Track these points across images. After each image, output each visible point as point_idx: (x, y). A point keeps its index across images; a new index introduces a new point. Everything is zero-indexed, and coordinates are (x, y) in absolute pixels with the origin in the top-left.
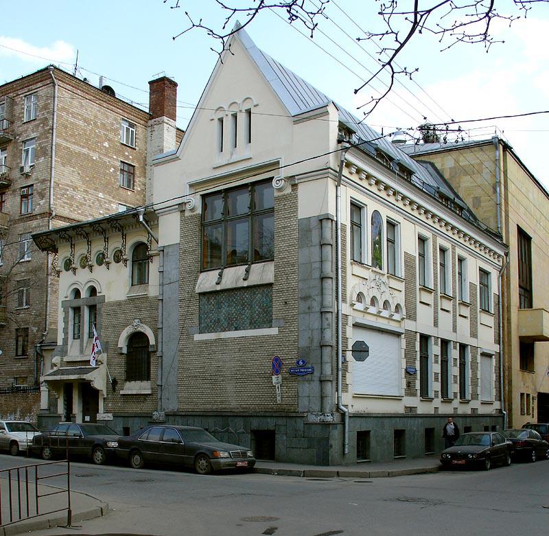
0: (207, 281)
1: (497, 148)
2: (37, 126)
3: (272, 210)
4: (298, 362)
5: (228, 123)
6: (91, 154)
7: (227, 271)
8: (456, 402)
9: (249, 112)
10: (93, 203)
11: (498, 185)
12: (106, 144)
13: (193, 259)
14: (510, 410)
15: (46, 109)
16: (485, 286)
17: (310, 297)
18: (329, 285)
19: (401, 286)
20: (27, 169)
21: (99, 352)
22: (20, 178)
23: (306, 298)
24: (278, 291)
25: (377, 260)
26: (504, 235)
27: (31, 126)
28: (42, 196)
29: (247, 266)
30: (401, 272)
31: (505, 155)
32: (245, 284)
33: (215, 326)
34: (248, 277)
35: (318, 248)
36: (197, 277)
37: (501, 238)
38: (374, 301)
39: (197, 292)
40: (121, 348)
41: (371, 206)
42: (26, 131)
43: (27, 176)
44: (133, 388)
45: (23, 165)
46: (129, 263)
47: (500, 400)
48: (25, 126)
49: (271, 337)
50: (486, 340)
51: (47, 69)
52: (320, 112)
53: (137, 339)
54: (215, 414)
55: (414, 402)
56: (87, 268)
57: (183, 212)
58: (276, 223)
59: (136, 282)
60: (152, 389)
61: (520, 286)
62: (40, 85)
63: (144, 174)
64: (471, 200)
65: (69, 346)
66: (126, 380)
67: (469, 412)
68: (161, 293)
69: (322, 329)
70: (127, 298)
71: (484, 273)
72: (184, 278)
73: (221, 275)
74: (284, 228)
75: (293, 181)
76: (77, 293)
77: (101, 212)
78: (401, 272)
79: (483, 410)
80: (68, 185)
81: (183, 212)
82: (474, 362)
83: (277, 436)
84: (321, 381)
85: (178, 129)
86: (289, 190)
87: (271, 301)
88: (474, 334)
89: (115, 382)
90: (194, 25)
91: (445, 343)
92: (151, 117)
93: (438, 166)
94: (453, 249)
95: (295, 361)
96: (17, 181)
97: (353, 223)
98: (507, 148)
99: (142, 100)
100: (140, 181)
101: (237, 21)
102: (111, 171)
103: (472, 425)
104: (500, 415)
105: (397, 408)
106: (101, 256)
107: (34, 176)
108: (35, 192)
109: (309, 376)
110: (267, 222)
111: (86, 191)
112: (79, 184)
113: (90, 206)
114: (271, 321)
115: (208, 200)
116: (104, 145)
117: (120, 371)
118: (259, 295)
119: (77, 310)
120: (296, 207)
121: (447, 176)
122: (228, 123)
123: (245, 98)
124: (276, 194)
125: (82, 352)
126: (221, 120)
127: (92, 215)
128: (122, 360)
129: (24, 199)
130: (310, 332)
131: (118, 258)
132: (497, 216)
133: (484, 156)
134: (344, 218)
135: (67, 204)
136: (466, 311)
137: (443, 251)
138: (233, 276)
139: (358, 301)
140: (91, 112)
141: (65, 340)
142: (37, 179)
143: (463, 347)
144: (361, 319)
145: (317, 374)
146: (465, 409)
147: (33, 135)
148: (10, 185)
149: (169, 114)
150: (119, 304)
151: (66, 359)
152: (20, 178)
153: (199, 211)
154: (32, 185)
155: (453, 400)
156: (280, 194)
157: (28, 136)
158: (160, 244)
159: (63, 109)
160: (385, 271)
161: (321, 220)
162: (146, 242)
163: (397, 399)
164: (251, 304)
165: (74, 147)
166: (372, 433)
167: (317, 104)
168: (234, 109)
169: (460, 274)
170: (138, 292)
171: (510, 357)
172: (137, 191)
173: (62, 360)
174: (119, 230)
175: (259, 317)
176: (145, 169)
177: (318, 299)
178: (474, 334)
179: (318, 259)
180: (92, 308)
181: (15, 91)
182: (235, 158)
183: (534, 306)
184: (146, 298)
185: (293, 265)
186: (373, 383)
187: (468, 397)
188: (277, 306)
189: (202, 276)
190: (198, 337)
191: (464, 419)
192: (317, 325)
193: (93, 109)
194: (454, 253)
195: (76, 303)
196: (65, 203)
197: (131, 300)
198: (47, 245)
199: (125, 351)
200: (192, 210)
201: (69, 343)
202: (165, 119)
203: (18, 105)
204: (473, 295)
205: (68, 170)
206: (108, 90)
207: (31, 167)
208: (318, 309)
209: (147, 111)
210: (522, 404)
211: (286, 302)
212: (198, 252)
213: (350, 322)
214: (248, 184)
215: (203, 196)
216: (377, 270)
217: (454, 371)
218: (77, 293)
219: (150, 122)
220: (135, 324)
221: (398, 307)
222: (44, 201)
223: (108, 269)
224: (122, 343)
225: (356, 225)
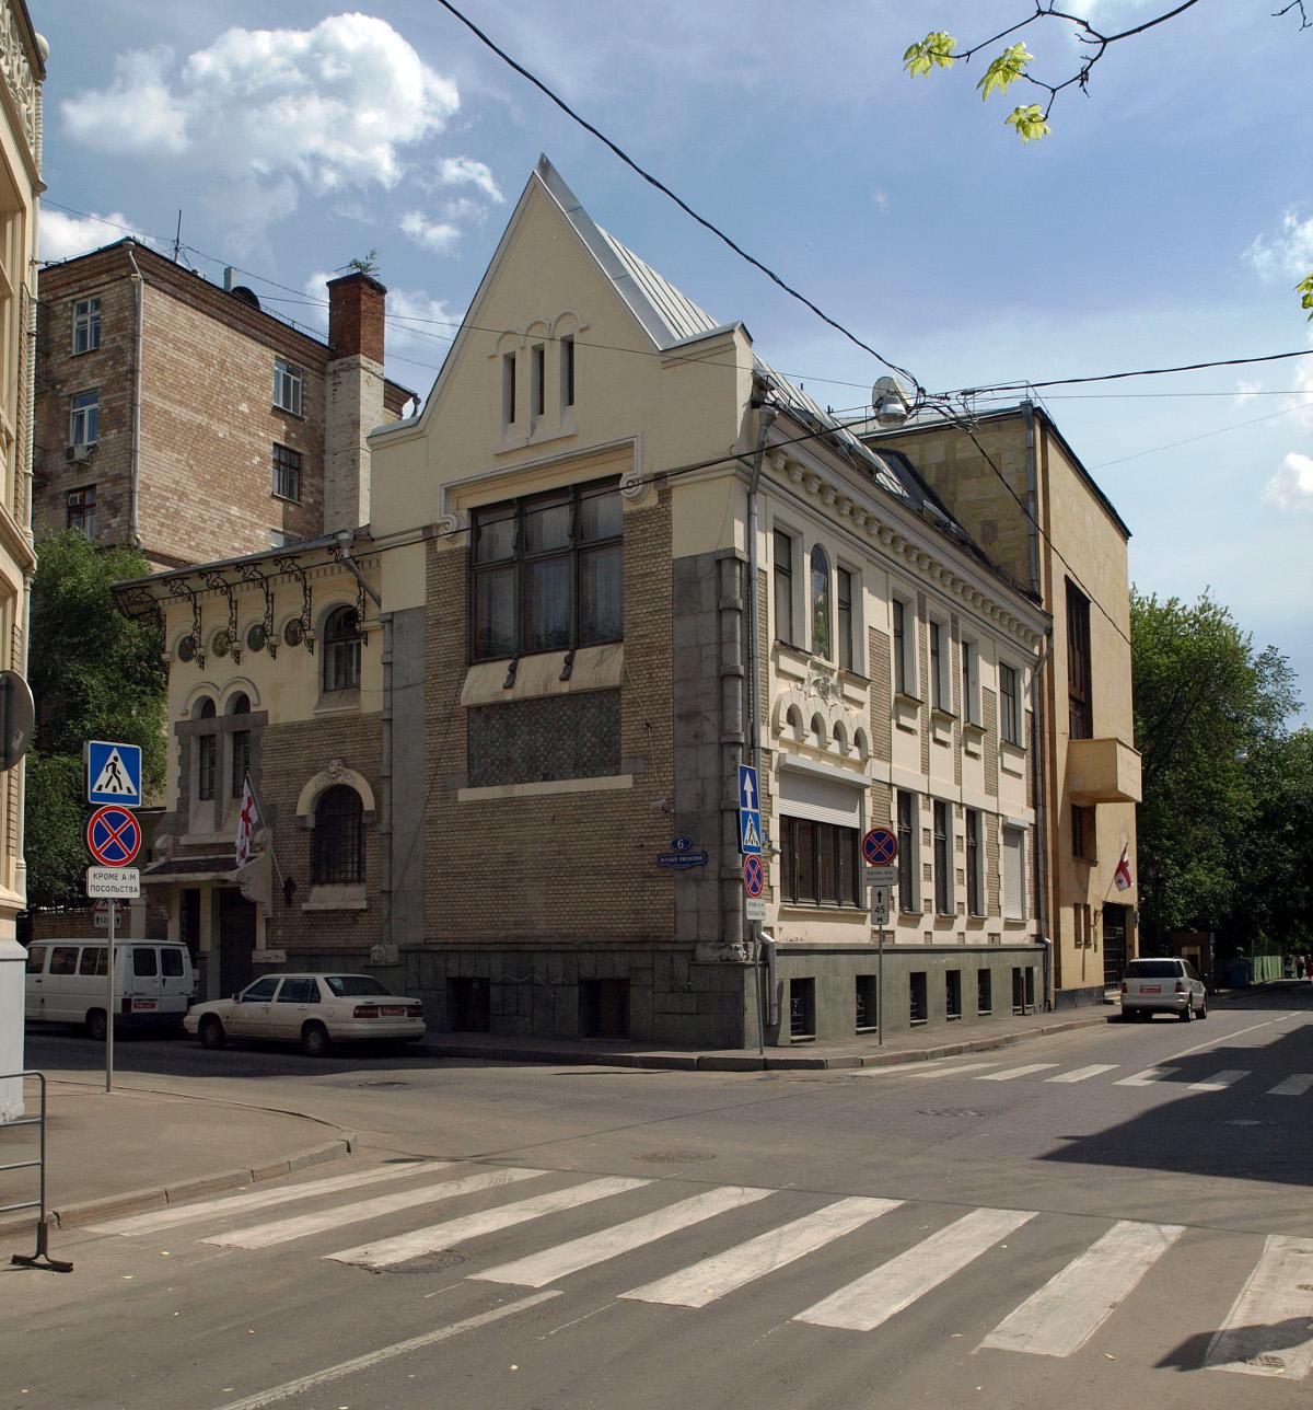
0: (484, 683)
2: (101, 365)
3: (616, 541)
4: (674, 844)
6: (215, 426)
7: (524, 662)
9: (569, 345)
10: (220, 527)
11: (1028, 501)
12: (244, 407)
13: (453, 639)
15: (119, 330)
20: (80, 454)
21: (258, 826)
22: (66, 471)
23: (689, 716)
24: (632, 702)
25: (822, 640)
26: (1043, 596)
27: (87, 364)
28: (114, 508)
29: (567, 653)
32: (565, 688)
33: (504, 771)
34: (513, 682)
35: (714, 615)
36: (463, 675)
37: (1038, 600)
39: (462, 704)
40: (303, 818)
41: (811, 535)
42: (77, 373)
43: (81, 466)
44: (327, 897)
45: (72, 444)
48: (75, 364)
49: (619, 793)
50: (1014, 803)
51: (118, 245)
53: (337, 800)
54: (504, 947)
56: (228, 655)
60: (369, 900)
61: (1071, 697)
62: (105, 278)
63: (320, 470)
64: (978, 527)
65: (191, 813)
68: (388, 705)
69: (722, 777)
70: (313, 717)
72: (435, 676)
73: (513, 670)
76: (207, 707)
77: (236, 545)
80: (167, 489)
84: (721, 881)
85: (387, 381)
86: (651, 500)
87: (618, 722)
89: (290, 886)
90: (1105, 41)
91: (941, 808)
93: (914, 460)
94: (955, 620)
95: (668, 841)
96: (58, 477)
97: (778, 569)
98: (1048, 427)
99: (316, 319)
100: (312, 485)
101: (543, 155)
102: (255, 462)
103: (991, 967)
104: (1039, 945)
106: (258, 631)
107: (96, 468)
108: (99, 501)
109: (696, 871)
111: (203, 502)
112: (191, 486)
113: (213, 533)
114: (618, 762)
115: (482, 520)
116: (240, 408)
117: (299, 861)
118: (593, 710)
119: (207, 741)
120: (669, 534)
121: (930, 480)
123: (563, 311)
125: (218, 825)
126: (511, 361)
127: (217, 551)
128: (305, 840)
129: (75, 515)
130: (700, 783)
131: (294, 635)
132: (1029, 558)
133: (1000, 443)
134: (765, 556)
135: (168, 527)
138: (539, 674)
140: (213, 339)
141: (183, 803)
142: (104, 474)
143: (973, 816)
144: (804, 761)
145: (713, 865)
146: (978, 938)
147: (93, 383)
148: (45, 485)
149: (370, 349)
150: (297, 729)
151: (184, 840)
152: (66, 471)
154: (92, 487)
155: (956, 917)
156: (634, 508)
157: (81, 384)
158: (387, 607)
159: (158, 332)
160: (835, 664)
161: (719, 562)
162: (355, 604)
164: (578, 732)
165: (176, 410)
166: (817, 982)
167: (704, 329)
169: (966, 670)
170: (338, 708)
172: (308, 504)
173: (176, 842)
174: (297, 579)
175: (593, 753)
176: (323, 461)
177: (713, 716)
178: (992, 789)
179: (713, 638)
180: (240, 738)
181: (51, 290)
182: (542, 434)
183: (1095, 734)
184: (355, 719)
185: (663, 651)
188: (629, 733)
189: (475, 673)
190: (466, 795)
191: (977, 955)
192: (711, 769)
193: (214, 335)
195: (206, 727)
196: (162, 525)
197: (321, 724)
198: (141, 608)
199: (311, 823)
201: (192, 807)
202: (363, 360)
203: (57, 318)
205: (167, 457)
206: (246, 297)
207: (89, 448)
208: (714, 738)
209: (326, 342)
210: (1077, 924)
211: (648, 725)
214: (510, 500)
215: (475, 512)
216: (821, 660)
217: (959, 860)
218: (207, 707)
219: (333, 366)
220: (333, 769)
222: (118, 519)
223: (275, 657)
224: (304, 806)
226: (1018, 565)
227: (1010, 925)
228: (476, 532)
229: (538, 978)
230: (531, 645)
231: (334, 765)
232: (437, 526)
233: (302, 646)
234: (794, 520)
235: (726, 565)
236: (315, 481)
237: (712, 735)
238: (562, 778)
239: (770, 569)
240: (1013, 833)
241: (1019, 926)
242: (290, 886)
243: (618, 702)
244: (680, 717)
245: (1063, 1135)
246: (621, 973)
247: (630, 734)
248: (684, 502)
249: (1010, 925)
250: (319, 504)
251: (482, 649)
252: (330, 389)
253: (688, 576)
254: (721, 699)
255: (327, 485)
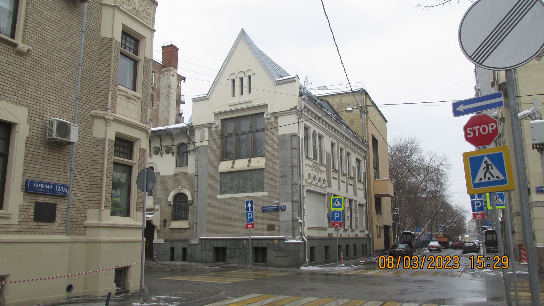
0: (225, 166)
1: (362, 94)
5: (237, 82)
8: (349, 231)
9: (250, 77)
13: (216, 154)
14: (372, 235)
16: (359, 167)
17: (286, 176)
18: (296, 169)
19: (324, 169)
23: (283, 177)
25: (315, 155)
30: (325, 162)
31: (366, 98)
33: (231, 190)
35: (290, 150)
38: (315, 177)
41: (312, 128)
44: (175, 224)
46: (175, 154)
47: (368, 229)
49: (263, 197)
50: (360, 198)
52: (292, 80)
53: (180, 197)
55: (331, 231)
57: (210, 128)
58: (267, 136)
59: (178, 165)
66: (172, 220)
67: (355, 236)
71: (358, 161)
73: (233, 163)
74: (271, 139)
75: (276, 115)
78: (325, 162)
79: (361, 235)
81: (210, 128)
82: (356, 209)
83: (268, 250)
86: (273, 120)
87: (264, 178)
88: (355, 194)
89: (165, 221)
92: (163, 67)
93: (331, 103)
94: (346, 149)
98: (366, 94)
105: (324, 234)
110: (258, 135)
114: (263, 188)
117: (168, 214)
121: (335, 108)
122: (237, 82)
124: (266, 121)
126: (233, 81)
128: (171, 208)
134: (302, 135)
136: (351, 182)
137: (341, 150)
138: (241, 164)
139: (309, 178)
143: (351, 201)
144: (312, 188)
146: (352, 235)
150: (168, 177)
153: (220, 128)
156: (268, 121)
161: (291, 136)
163: (324, 229)
168: (242, 75)
171: (371, 205)
177: (290, 177)
178: (355, 194)
184: (185, 174)
186: (314, 220)
187: (354, 228)
188: (267, 180)
190: (219, 196)
194: (346, 151)
197: (176, 174)
199: (172, 204)
200: (216, 127)
202: (172, 68)
204: (354, 173)
208: (290, 183)
212: (219, 150)
213: (305, 190)
215: (222, 120)
221: (324, 180)
224: (170, 199)
225: (306, 138)
226: (360, 132)
227: (362, 231)
228: (223, 126)
229: (241, 247)
230: (238, 157)
231: (180, 188)
232: (212, 124)
233: (171, 154)
234: (308, 124)
235: (293, 137)
236: (157, 102)
237: (290, 182)
238: (248, 192)
239: (303, 137)
240: (361, 205)
241: (363, 231)
242: (165, 221)
243: (264, 172)
244: (281, 177)
245: (527, 193)
246: (265, 245)
247: (267, 181)
248: (282, 121)
249: (362, 231)
250: (158, 109)
251: (225, 156)
252: (162, 76)
253: (283, 139)
254: (292, 172)
255: (160, 103)
